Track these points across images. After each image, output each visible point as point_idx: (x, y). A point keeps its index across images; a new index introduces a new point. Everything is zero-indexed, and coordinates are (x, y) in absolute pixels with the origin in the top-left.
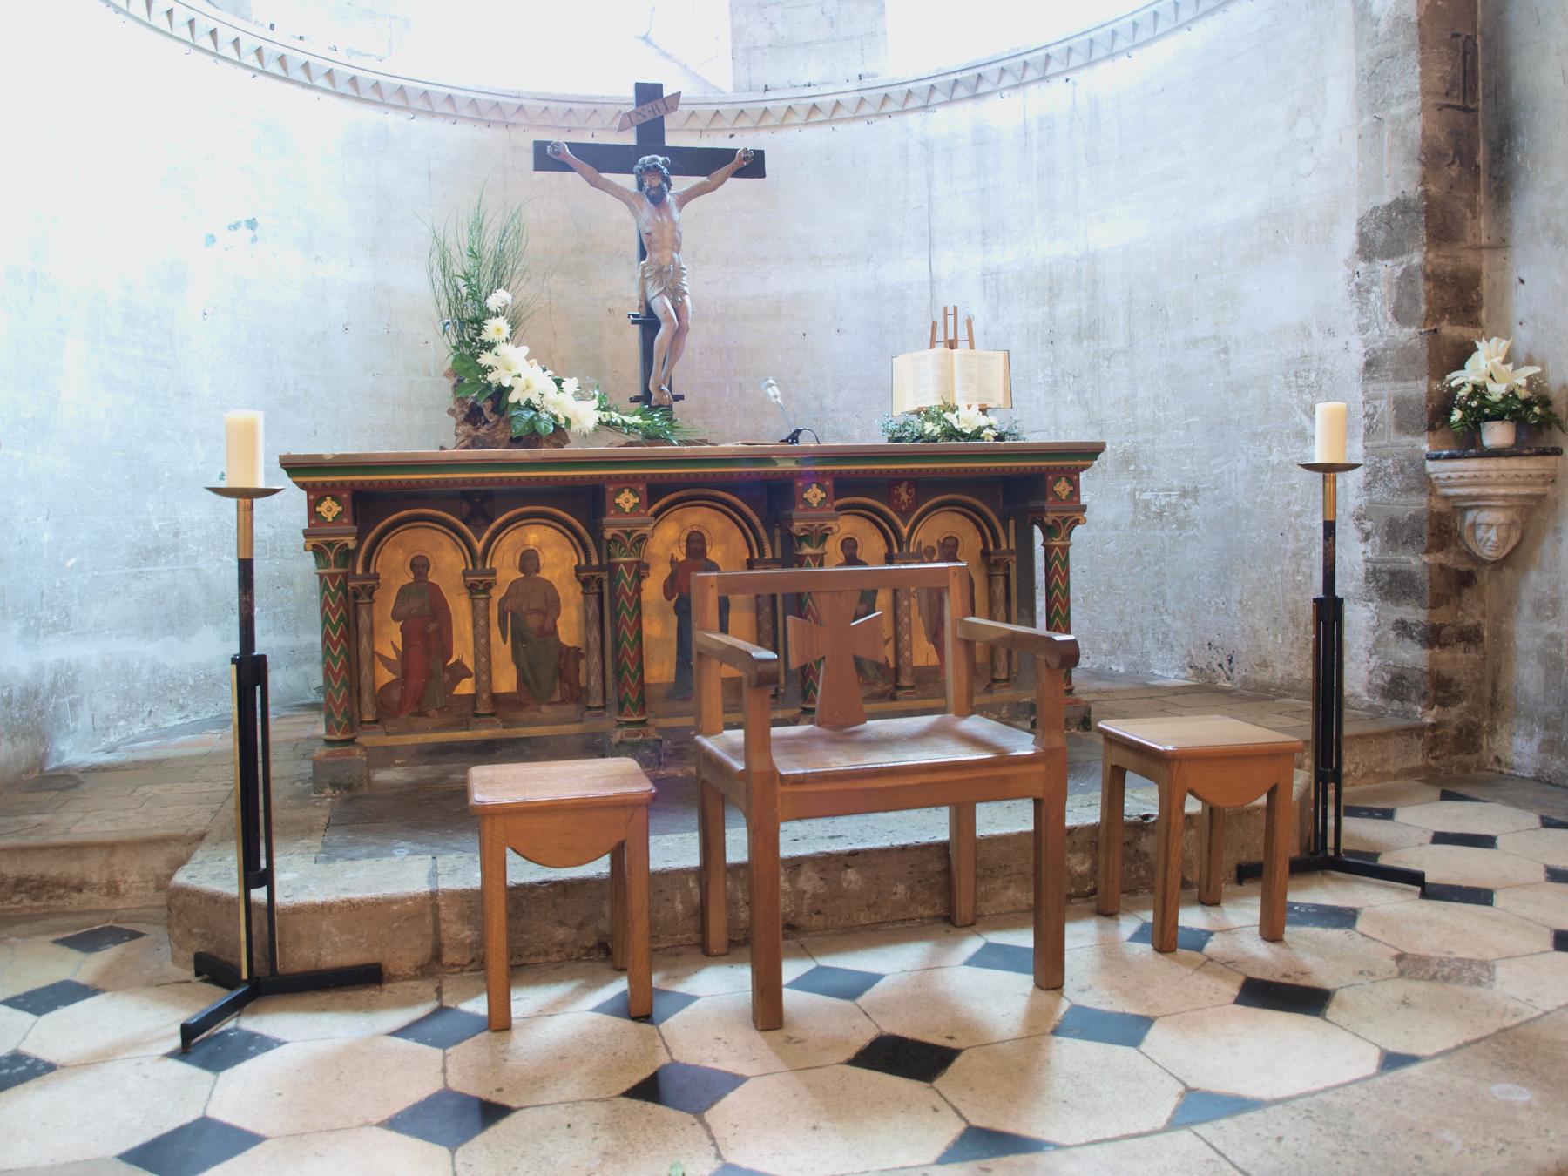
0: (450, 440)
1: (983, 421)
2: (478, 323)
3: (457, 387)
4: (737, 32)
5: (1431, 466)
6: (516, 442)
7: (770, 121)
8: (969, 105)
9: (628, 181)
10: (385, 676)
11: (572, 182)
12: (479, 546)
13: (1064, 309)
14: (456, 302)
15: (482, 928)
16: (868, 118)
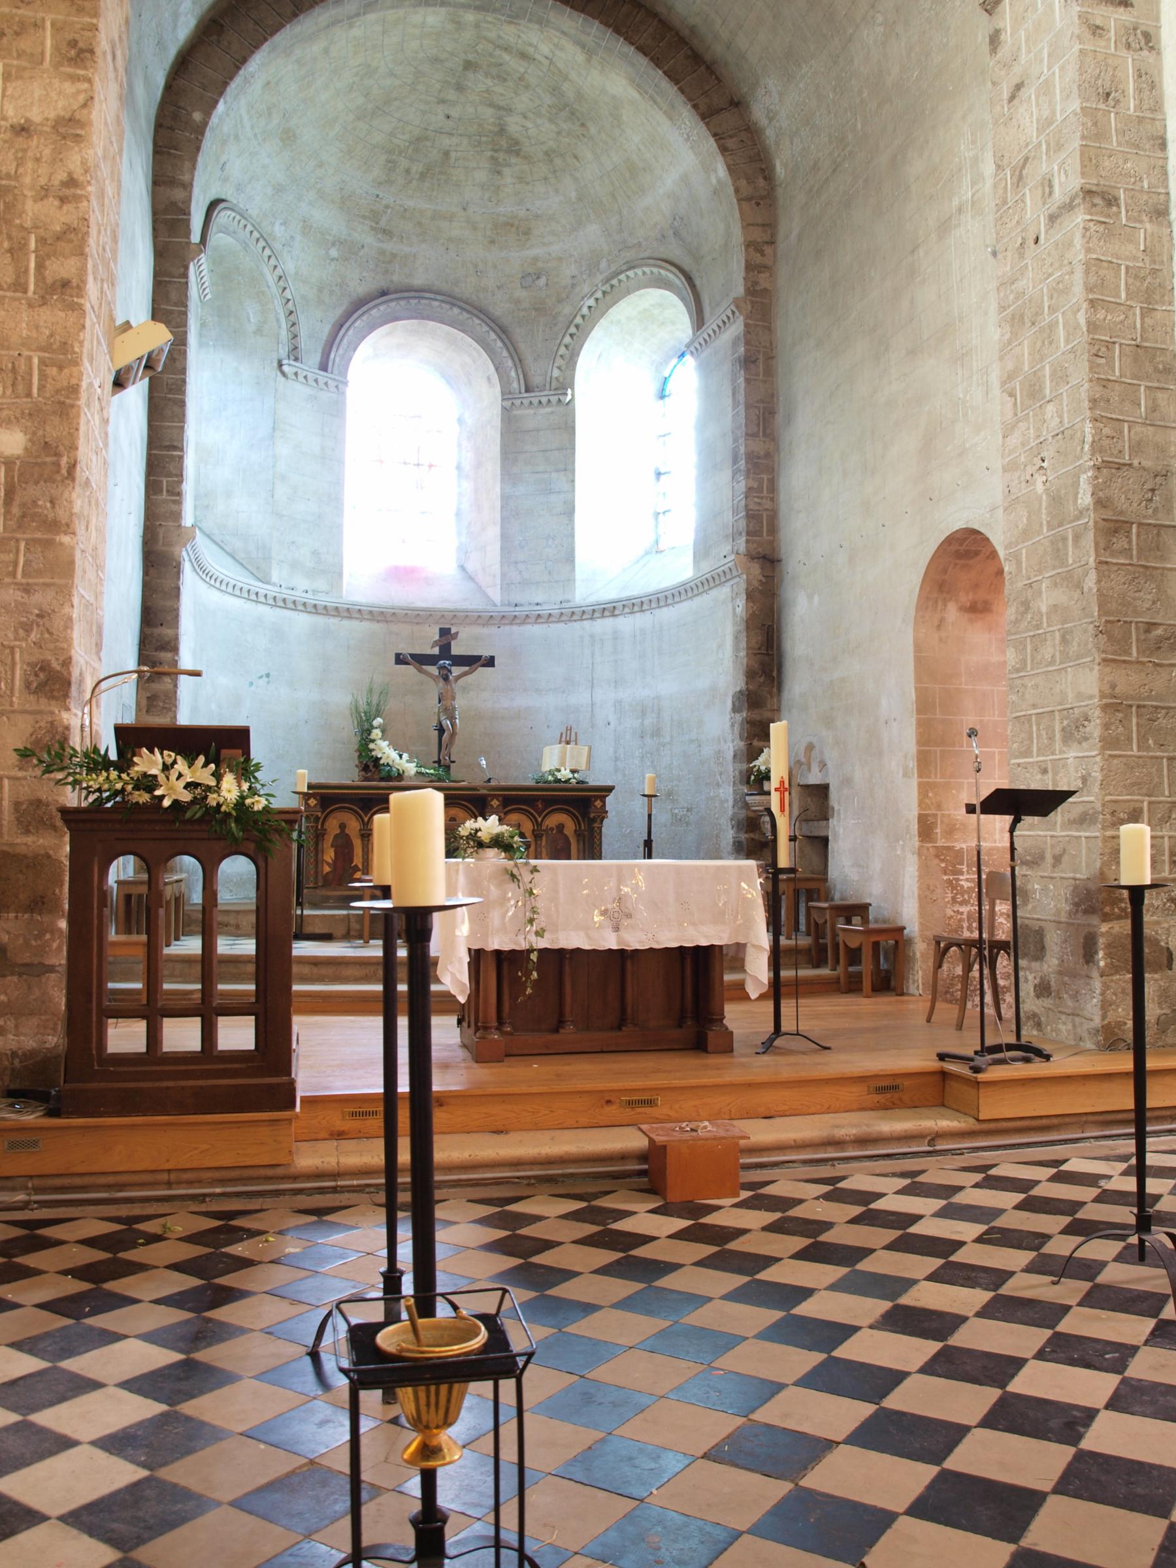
0: (357, 778)
1: (571, 776)
2: (369, 732)
3: (360, 756)
4: (503, 575)
5: (748, 798)
6: (382, 779)
7: (518, 621)
8: (611, 619)
9: (433, 670)
10: (327, 869)
11: (410, 670)
12: (366, 819)
13: (647, 722)
14: (360, 722)
15: (362, 925)
16: (565, 622)
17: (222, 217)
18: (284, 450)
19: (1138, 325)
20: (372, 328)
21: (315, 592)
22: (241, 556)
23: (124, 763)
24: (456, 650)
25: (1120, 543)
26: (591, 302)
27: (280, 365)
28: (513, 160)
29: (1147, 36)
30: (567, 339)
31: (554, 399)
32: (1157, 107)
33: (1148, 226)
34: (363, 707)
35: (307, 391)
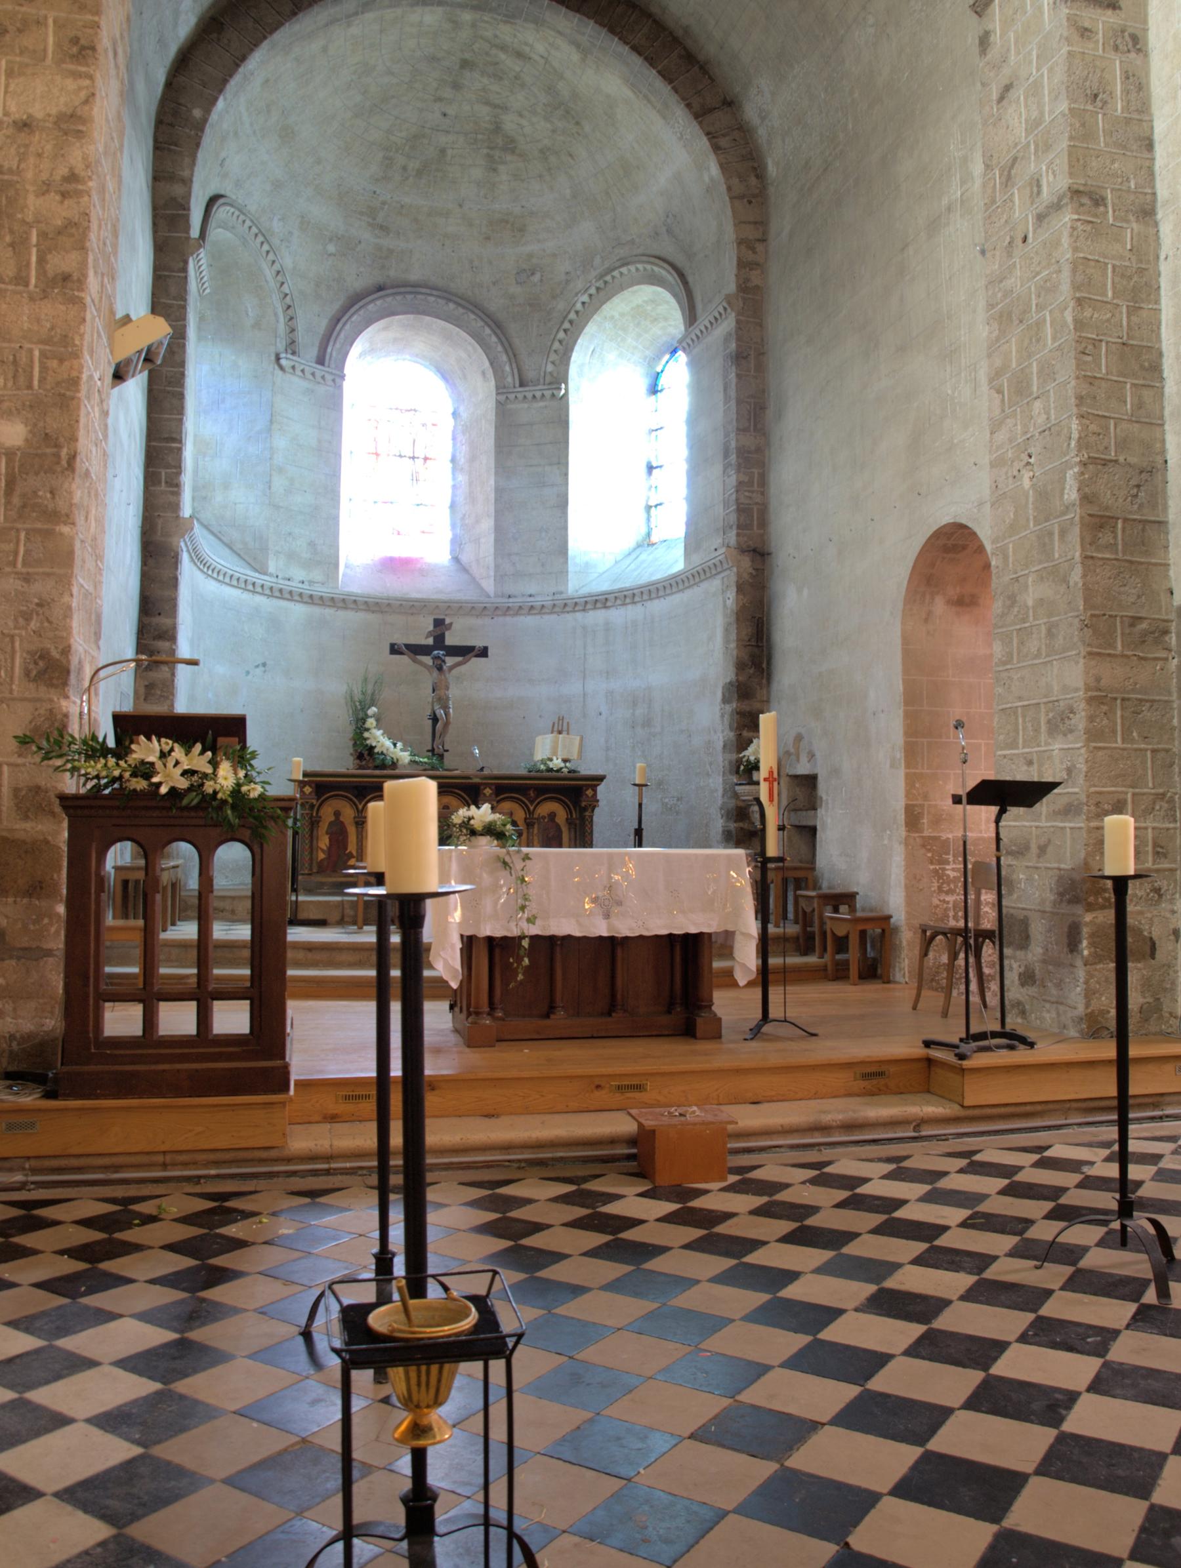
0: (351, 766)
1: (562, 765)
2: (364, 720)
3: (355, 745)
4: (497, 567)
5: (737, 788)
6: (376, 768)
8: (603, 611)
9: (427, 660)
10: (322, 856)
11: (404, 660)
12: (360, 807)
14: (355, 712)
15: (356, 911)
16: (557, 613)
17: (221, 213)
18: (280, 442)
19: (1125, 323)
20: (368, 323)
21: (311, 582)
22: (238, 546)
23: (121, 751)
24: (450, 640)
25: (1106, 538)
26: (585, 298)
27: (278, 358)
28: (509, 158)
29: (1135, 39)
30: (561, 335)
31: (548, 393)
32: (1144, 108)
33: (1135, 225)
34: (358, 696)
35: (305, 384)
